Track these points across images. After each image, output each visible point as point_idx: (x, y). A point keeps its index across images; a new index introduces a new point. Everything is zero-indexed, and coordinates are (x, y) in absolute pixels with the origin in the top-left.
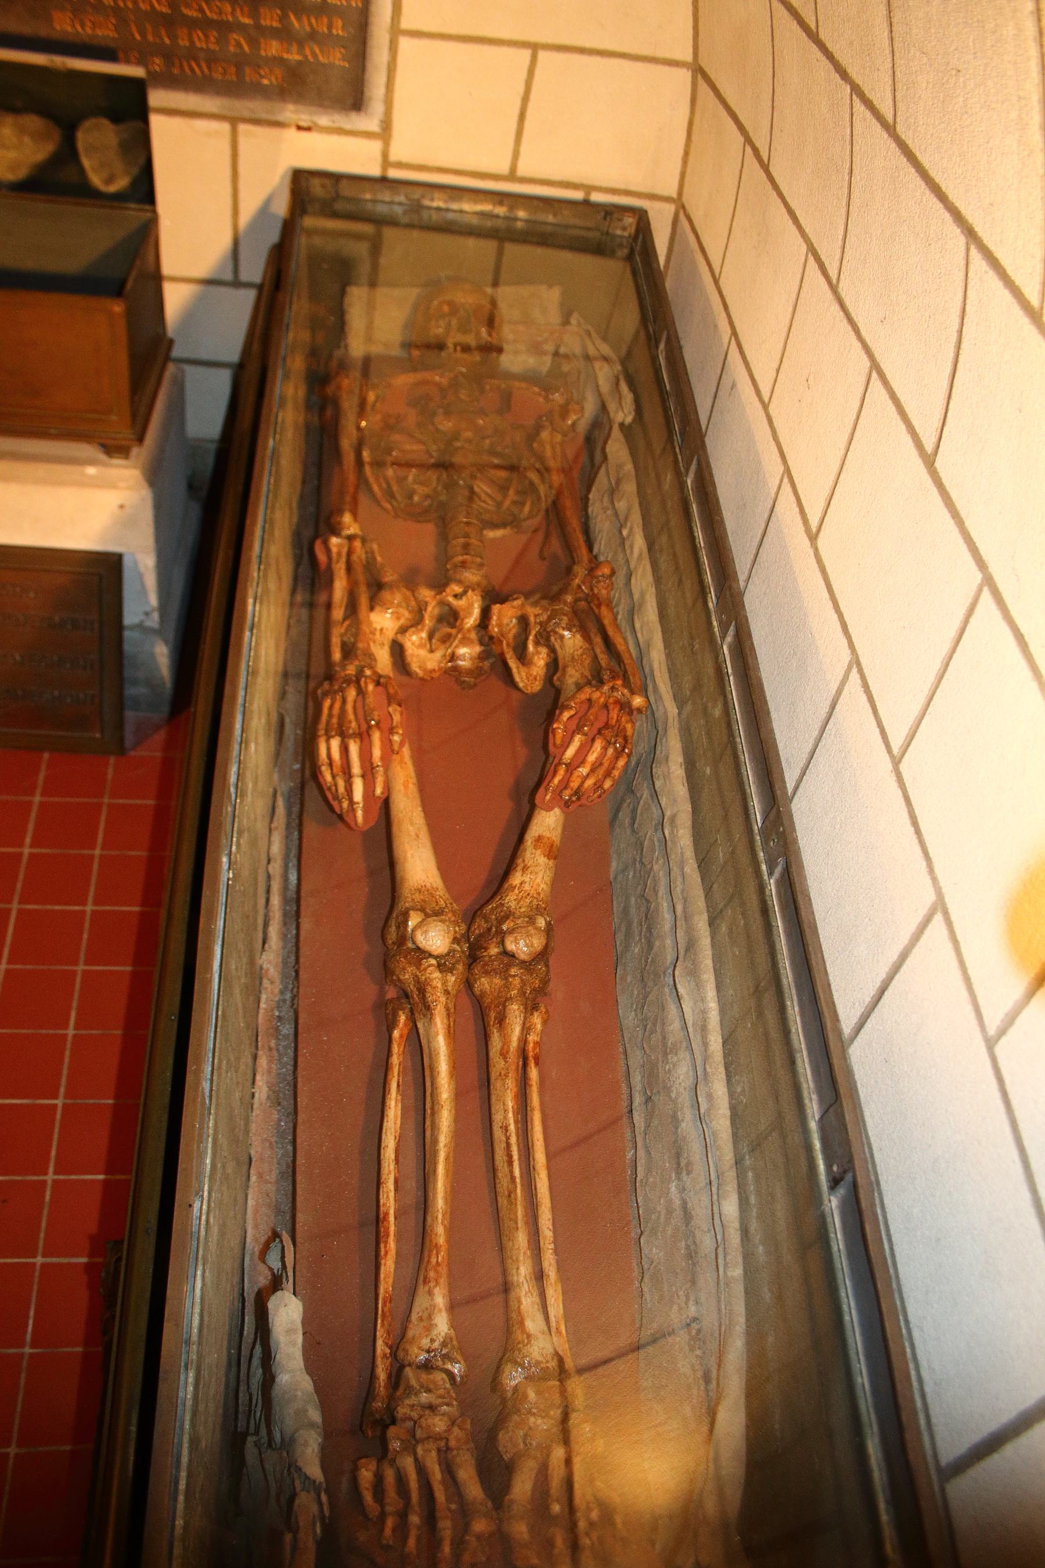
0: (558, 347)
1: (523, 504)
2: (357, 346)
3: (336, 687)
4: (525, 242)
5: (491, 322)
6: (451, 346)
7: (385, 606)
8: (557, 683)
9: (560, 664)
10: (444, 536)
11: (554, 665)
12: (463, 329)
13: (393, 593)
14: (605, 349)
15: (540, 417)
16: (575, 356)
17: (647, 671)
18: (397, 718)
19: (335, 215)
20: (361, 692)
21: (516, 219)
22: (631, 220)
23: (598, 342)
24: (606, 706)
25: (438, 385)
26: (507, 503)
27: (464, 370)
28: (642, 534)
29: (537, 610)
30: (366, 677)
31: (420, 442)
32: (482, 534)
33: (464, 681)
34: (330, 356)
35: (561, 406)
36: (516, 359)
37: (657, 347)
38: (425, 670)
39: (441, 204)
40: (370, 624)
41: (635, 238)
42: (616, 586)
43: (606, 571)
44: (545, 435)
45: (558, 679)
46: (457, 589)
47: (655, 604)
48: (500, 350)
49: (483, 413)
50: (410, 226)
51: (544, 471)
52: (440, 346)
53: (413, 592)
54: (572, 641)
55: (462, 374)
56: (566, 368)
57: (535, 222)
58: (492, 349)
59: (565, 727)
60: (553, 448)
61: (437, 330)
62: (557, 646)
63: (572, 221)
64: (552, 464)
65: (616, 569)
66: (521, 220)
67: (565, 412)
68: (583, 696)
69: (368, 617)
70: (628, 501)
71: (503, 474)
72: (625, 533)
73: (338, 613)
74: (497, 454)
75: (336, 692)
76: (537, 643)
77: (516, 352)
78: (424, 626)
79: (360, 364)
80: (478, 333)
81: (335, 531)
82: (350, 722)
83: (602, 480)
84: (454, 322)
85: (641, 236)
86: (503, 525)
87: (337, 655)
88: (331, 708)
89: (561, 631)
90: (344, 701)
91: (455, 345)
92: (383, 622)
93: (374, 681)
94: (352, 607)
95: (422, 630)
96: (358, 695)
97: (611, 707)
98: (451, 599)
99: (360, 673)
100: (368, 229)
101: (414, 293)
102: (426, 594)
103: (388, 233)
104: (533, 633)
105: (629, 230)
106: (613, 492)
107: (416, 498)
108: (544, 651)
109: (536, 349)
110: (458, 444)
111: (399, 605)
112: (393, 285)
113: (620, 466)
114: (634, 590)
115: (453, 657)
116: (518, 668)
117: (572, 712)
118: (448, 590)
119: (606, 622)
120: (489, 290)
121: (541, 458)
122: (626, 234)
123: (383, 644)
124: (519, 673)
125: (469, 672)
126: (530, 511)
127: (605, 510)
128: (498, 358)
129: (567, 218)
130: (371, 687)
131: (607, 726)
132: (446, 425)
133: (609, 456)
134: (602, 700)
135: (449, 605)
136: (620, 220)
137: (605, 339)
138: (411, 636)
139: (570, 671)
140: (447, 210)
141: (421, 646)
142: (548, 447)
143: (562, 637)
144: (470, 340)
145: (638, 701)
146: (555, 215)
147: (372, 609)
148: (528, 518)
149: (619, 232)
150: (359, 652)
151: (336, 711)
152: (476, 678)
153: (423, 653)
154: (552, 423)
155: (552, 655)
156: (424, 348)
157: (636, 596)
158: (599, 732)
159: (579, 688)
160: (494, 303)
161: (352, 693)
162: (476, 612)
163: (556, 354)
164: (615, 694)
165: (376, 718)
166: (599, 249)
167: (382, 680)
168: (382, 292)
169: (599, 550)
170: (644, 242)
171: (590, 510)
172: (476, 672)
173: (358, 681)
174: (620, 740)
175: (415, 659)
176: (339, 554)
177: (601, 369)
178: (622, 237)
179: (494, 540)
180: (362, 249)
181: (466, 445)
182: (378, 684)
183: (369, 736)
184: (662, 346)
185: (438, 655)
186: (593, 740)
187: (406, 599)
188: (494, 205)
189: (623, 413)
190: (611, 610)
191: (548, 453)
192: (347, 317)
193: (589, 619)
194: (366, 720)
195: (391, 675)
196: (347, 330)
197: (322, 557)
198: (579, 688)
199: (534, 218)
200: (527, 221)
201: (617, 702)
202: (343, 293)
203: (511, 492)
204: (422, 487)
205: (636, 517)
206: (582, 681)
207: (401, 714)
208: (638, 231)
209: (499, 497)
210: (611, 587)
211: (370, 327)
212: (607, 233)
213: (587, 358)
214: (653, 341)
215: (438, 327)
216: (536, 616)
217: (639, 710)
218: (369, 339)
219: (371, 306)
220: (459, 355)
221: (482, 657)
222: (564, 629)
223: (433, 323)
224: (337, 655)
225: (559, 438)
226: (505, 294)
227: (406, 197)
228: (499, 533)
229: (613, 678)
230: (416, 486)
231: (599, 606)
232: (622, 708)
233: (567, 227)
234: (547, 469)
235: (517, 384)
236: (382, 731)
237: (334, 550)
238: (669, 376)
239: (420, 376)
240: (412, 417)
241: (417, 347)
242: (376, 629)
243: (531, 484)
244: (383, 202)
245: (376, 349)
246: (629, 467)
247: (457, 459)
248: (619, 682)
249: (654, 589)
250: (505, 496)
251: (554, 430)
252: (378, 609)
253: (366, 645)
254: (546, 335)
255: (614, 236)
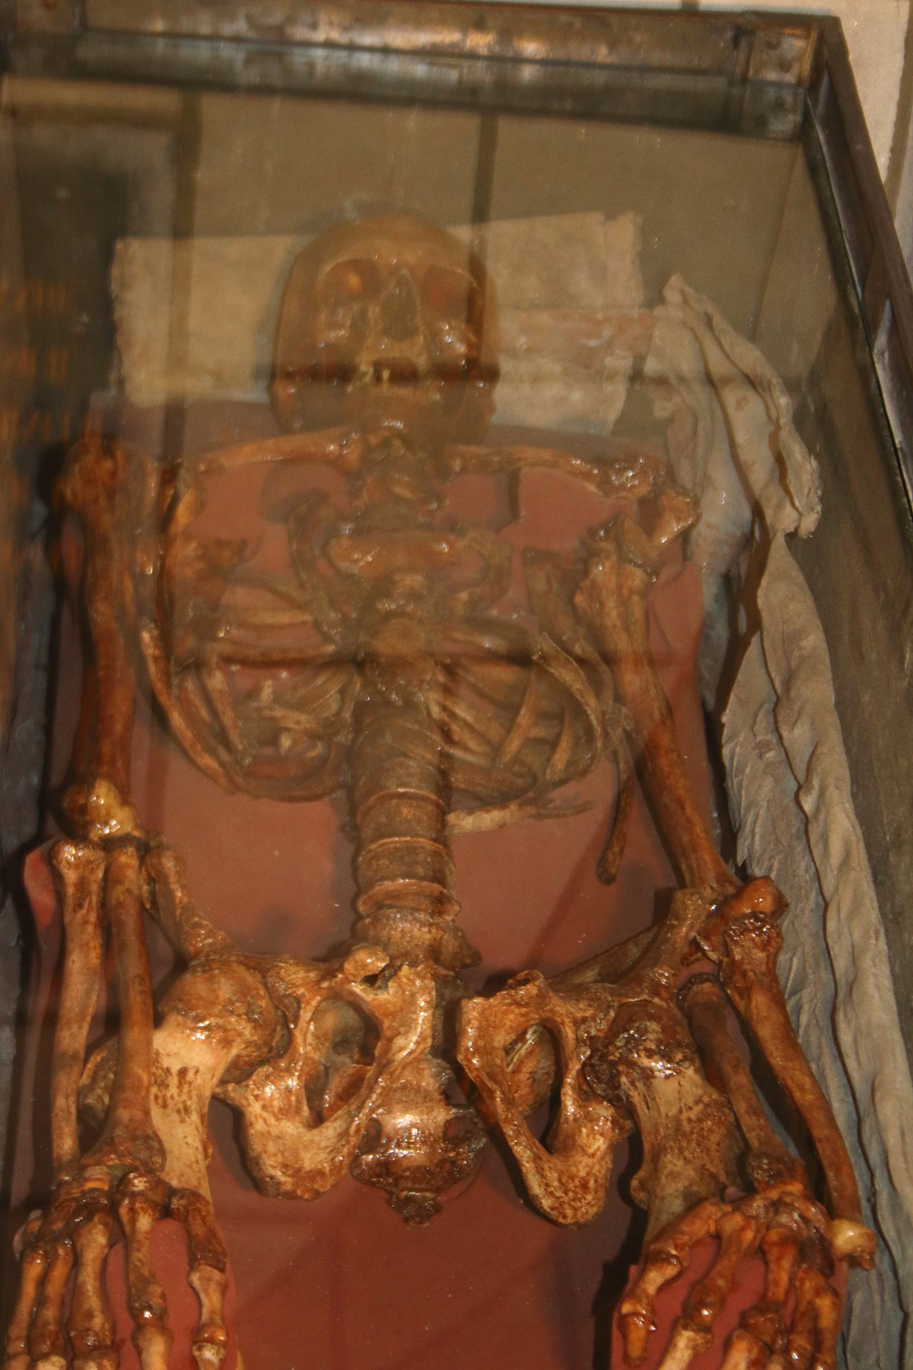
0: (639, 360)
1: (554, 745)
2: (147, 381)
3: (58, 1226)
4: (542, 112)
5: (474, 310)
6: (365, 367)
7: (194, 1014)
8: (640, 1196)
9: (647, 1146)
10: (353, 831)
11: (633, 1152)
12: (399, 326)
13: (211, 980)
14: (750, 356)
15: (592, 532)
16: (682, 379)
17: (874, 1156)
18: (211, 1301)
19: (83, 73)
20: (121, 1237)
21: (519, 60)
22: (799, 44)
23: (730, 338)
24: (760, 1251)
25: (336, 463)
26: (514, 745)
27: (399, 425)
28: (849, 806)
29: (583, 1009)
30: (134, 1196)
31: (300, 607)
32: (444, 824)
33: (408, 1199)
34: (83, 408)
35: (643, 502)
36: (535, 395)
37: (870, 345)
38: (297, 1173)
39: (336, 35)
40: (153, 1059)
41: (813, 86)
42: (789, 940)
43: (764, 902)
44: (599, 570)
45: (643, 1185)
46: (375, 962)
47: (886, 982)
48: (492, 375)
49: (453, 528)
50: (263, 90)
51: (600, 663)
52: (343, 373)
53: (264, 973)
54: (673, 1084)
55: (399, 435)
56: (662, 408)
57: (568, 63)
58: (478, 370)
59: (653, 1310)
60: (624, 602)
61: (334, 335)
62: (637, 1099)
63: (658, 57)
64: (621, 643)
65: (789, 897)
66: (531, 61)
67: (650, 513)
68: (699, 1227)
69: (149, 1042)
70: (814, 725)
71: (505, 674)
72: (808, 804)
73: (73, 1036)
74: (488, 626)
75: (57, 1239)
76: (585, 1096)
77: (537, 379)
78: (293, 1060)
79: (156, 424)
80: (434, 336)
81: (76, 828)
82: (90, 1315)
83: (751, 674)
84: (373, 312)
85: (825, 81)
86: (501, 800)
87: (66, 1143)
88: (43, 1281)
89: (646, 1062)
90: (76, 1262)
91: (378, 367)
92: (188, 1051)
93: (154, 1205)
94: (111, 1023)
95: (289, 1071)
96: (111, 1245)
97: (774, 1253)
98: (358, 988)
99: (121, 1185)
100: (165, 101)
101: (281, 248)
102: (295, 977)
103: (213, 108)
104: (575, 1067)
105: (795, 71)
106: (778, 705)
107: (286, 742)
108: (604, 1112)
109: (585, 365)
110: (387, 605)
111: (228, 1010)
112: (230, 228)
113: (791, 640)
114: (835, 949)
115: (374, 1136)
116: (536, 1158)
117: (670, 1271)
118: (348, 966)
119: (766, 1032)
120: (464, 233)
121: (596, 634)
122: (790, 78)
123: (187, 1110)
124: (540, 1171)
125: (421, 1175)
126: (571, 763)
127: (762, 748)
128: (488, 393)
129: (646, 49)
130: (144, 1222)
131: (764, 1304)
132: (361, 561)
133: (766, 620)
134: (749, 1235)
135: (355, 1004)
136: (772, 46)
137: (753, 336)
138: (261, 1085)
139: (672, 1162)
140: (352, 48)
141: (285, 1112)
142: (611, 604)
143: (648, 1075)
144: (417, 354)
145: (848, 1236)
146: (613, 46)
147: (158, 1021)
148: (562, 782)
149: (772, 75)
150: (119, 1132)
151: (54, 1289)
152: (438, 1190)
153: (291, 1128)
154: (619, 547)
155: (628, 1124)
156: (309, 376)
157: (841, 963)
158: (744, 1324)
159: (693, 1204)
160: (476, 267)
161: (96, 1239)
162: (424, 1016)
163: (636, 376)
164: (784, 1219)
165: (156, 1301)
166: (727, 118)
167: (176, 1203)
168: (201, 245)
169: (751, 849)
170: (833, 92)
171: (726, 751)
172: (441, 1174)
173: (112, 1210)
174: (801, 1341)
175: (271, 1147)
176: (82, 884)
177: (740, 405)
178: (779, 85)
179: (479, 836)
180: (151, 150)
181: (410, 608)
182: (165, 1212)
183: (139, 1351)
184: (881, 340)
185: (330, 1130)
186: (727, 1346)
187: (244, 991)
188: (465, 31)
189: (798, 512)
190: (778, 1000)
191: (612, 616)
192: (119, 313)
193: (719, 1026)
194: (131, 1309)
195: (205, 1191)
196: (120, 340)
197: (39, 895)
198: (693, 1204)
199: (561, 54)
200: (543, 62)
201: (791, 1240)
202: (107, 255)
203: (524, 717)
204: (298, 714)
205: (835, 764)
206: (700, 1189)
207: (224, 1289)
208: (818, 67)
209: (495, 731)
210: (772, 945)
211: (178, 332)
212: (744, 80)
213: (710, 381)
214: (861, 335)
215: (338, 326)
216: (578, 1023)
217: (853, 1260)
218: (177, 362)
219: (179, 282)
220: (386, 389)
221: (451, 1135)
222: (650, 1054)
223: (323, 317)
224: (66, 1143)
225: (637, 578)
226: (504, 236)
227: (249, 19)
228: (489, 819)
229: (778, 1177)
230: (278, 713)
231: (746, 993)
232: (802, 1255)
233: (645, 69)
234: (610, 659)
235: (530, 453)
236: (170, 1339)
237: (71, 876)
238: (900, 412)
239: (290, 444)
240: (275, 544)
241: (289, 376)
242: (168, 1071)
243: (566, 692)
244: (193, 36)
245: (197, 387)
246: (814, 639)
247: (387, 644)
248: (796, 1188)
249: (883, 945)
250: (510, 727)
251: (623, 559)
252: (173, 1019)
253: (138, 1114)
254: (607, 332)
255: (762, 85)
